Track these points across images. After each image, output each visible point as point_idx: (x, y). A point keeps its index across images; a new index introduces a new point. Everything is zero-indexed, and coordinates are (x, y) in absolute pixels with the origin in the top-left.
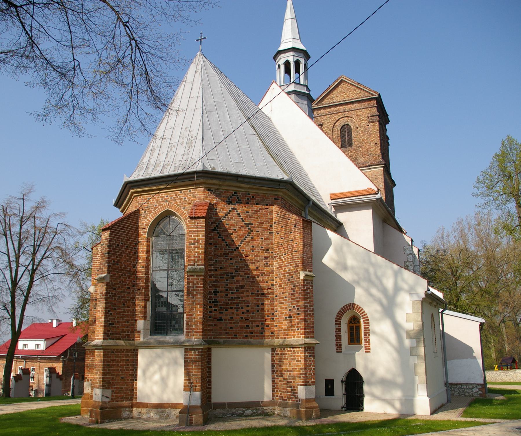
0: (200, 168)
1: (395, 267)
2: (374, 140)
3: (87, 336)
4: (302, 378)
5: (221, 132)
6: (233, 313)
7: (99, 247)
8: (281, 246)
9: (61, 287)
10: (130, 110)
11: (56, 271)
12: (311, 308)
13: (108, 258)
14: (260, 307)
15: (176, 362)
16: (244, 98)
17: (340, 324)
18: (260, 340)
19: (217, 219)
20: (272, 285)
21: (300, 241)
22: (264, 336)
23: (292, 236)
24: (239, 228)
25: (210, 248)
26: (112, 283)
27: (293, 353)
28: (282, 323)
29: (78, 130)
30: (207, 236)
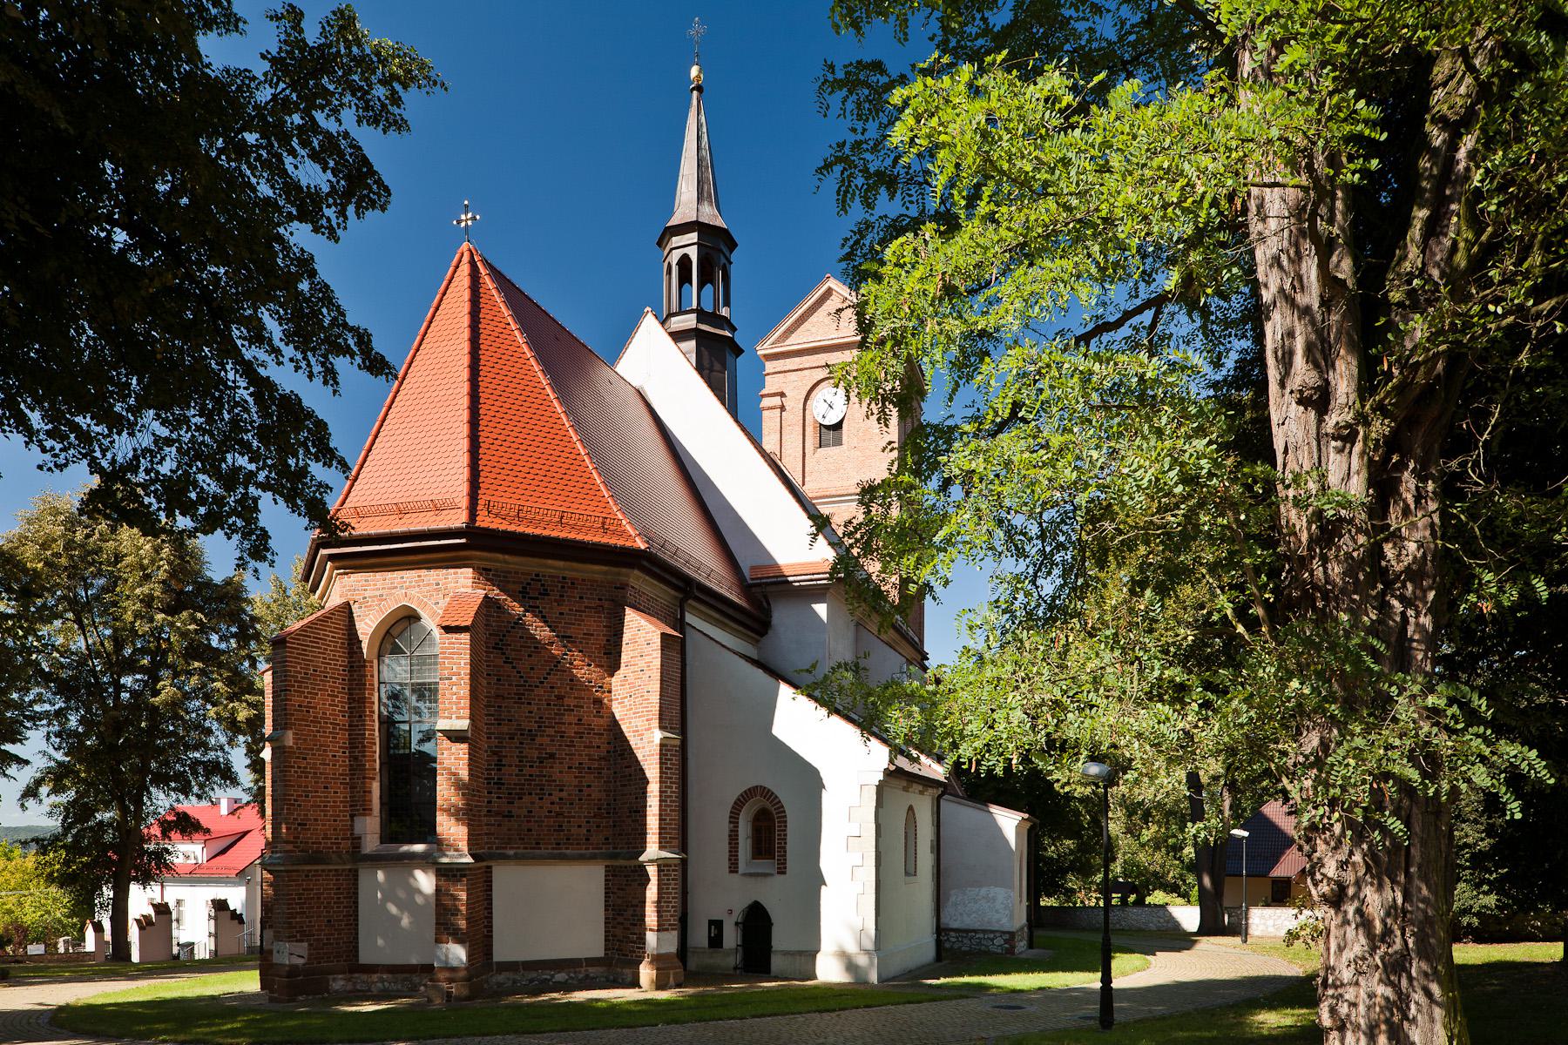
6: (533, 803)
26: (299, 748)
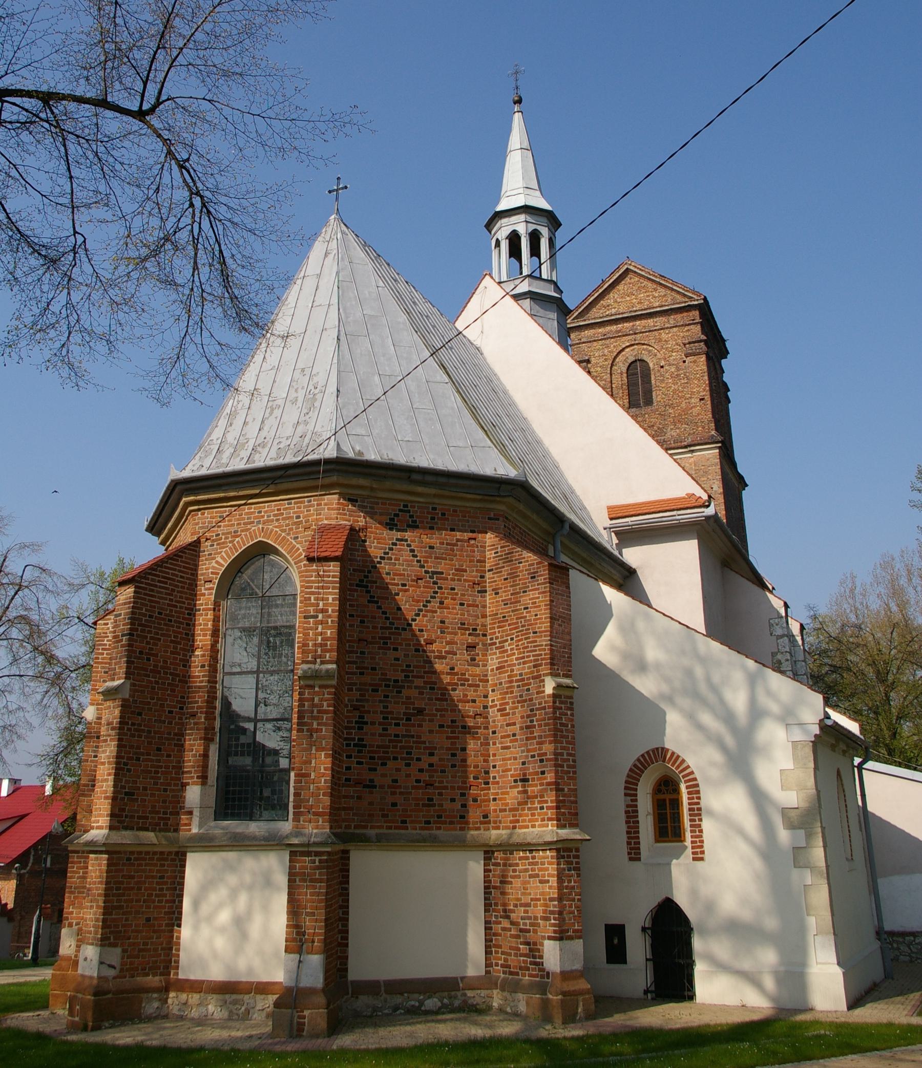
0: (330, 452)
1: (750, 663)
2: (699, 392)
3: (74, 818)
4: (553, 921)
5: (377, 378)
6: (398, 770)
7: (109, 619)
8: (503, 621)
9: (24, 705)
10: (187, 336)
11: (14, 670)
12: (571, 758)
13: (129, 645)
14: (459, 758)
15: (268, 883)
16: (424, 307)
17: (636, 795)
18: (459, 833)
19: (366, 561)
20: (485, 707)
21: (545, 610)
22: (467, 823)
23: (526, 599)
24: (413, 580)
25: (350, 626)
26: (135, 702)
27: (532, 864)
28: (507, 793)
29: (76, 373)
30: (343, 600)
